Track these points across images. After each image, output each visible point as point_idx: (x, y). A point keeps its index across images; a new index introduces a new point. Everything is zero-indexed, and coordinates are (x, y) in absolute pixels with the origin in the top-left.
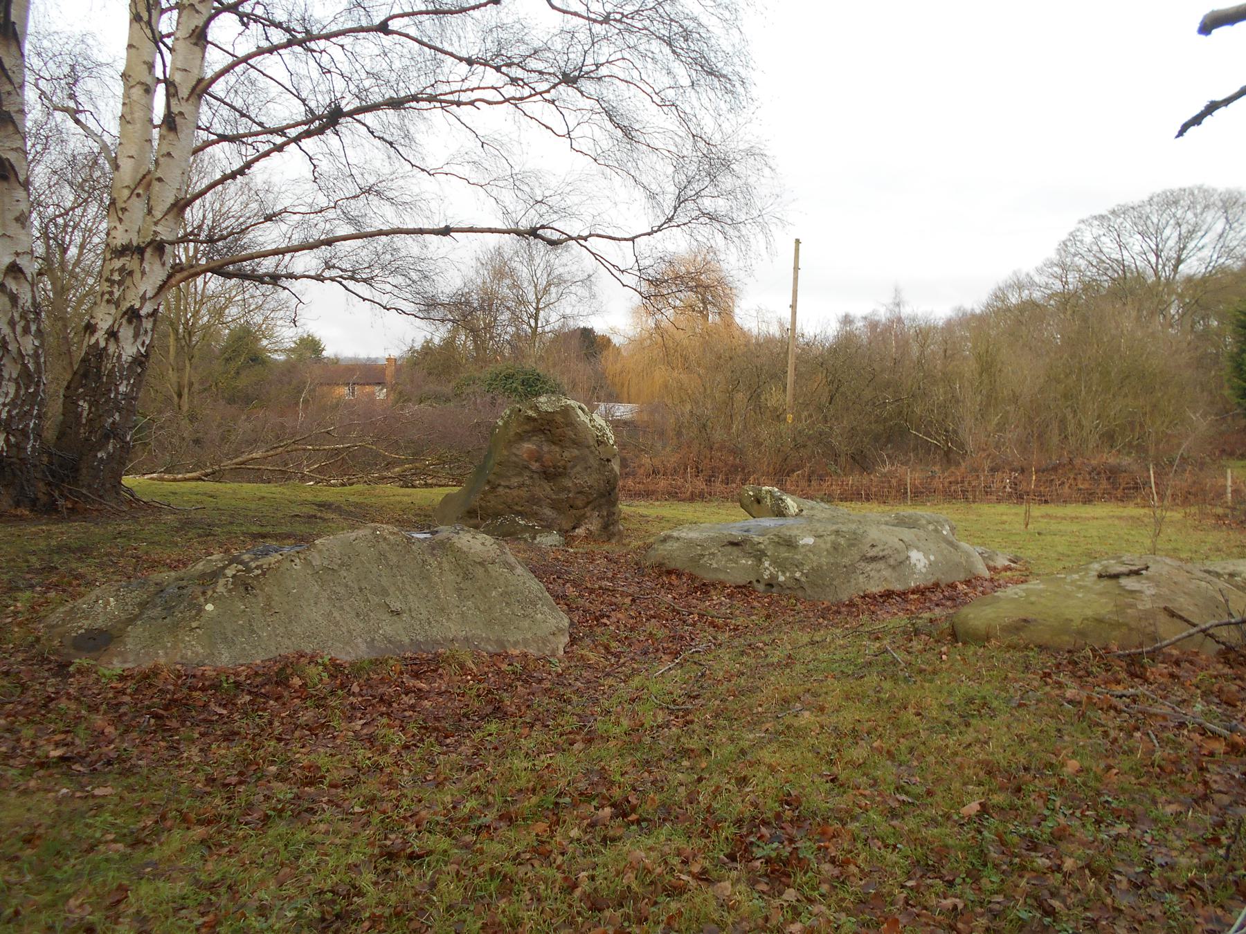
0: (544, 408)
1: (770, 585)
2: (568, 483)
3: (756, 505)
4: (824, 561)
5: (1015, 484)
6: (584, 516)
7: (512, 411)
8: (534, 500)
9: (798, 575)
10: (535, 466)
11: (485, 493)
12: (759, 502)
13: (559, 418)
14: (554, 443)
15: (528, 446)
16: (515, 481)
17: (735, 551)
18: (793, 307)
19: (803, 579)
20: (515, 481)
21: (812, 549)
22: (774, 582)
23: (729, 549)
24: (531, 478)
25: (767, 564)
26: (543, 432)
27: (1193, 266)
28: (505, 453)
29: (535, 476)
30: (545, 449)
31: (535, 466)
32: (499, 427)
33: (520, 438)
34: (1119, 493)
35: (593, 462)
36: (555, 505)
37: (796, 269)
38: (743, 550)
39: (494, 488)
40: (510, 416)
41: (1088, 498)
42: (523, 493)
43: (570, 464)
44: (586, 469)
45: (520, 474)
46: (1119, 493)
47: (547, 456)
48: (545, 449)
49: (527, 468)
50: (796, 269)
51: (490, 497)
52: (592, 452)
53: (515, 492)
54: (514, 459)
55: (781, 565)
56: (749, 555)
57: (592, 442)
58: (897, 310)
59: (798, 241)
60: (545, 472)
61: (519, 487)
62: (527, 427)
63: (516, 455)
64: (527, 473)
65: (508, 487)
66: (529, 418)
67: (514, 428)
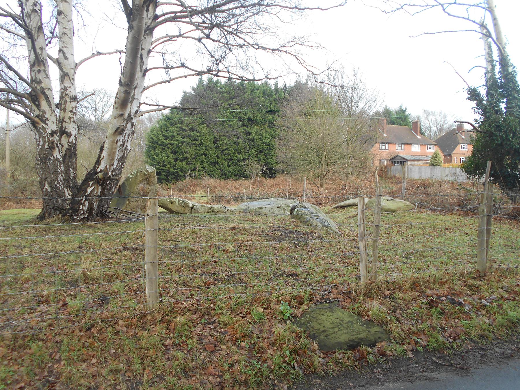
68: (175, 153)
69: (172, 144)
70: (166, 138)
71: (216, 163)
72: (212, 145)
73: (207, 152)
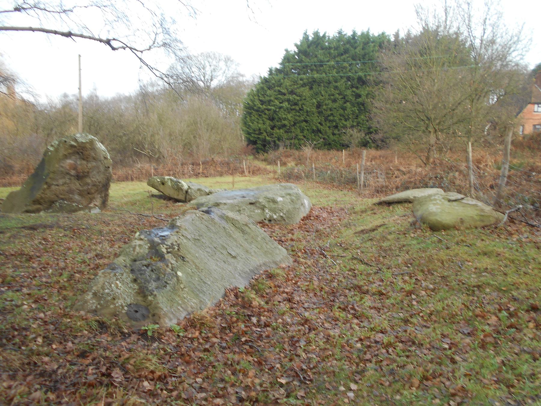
0: (80, 140)
1: (270, 221)
2: (88, 181)
3: (162, 186)
4: (290, 207)
5: (193, 170)
6: (94, 198)
7: (60, 142)
8: (71, 192)
9: (282, 214)
10: (73, 172)
11: (44, 190)
12: (163, 184)
13: (88, 146)
14: (84, 159)
15: (69, 161)
16: (61, 182)
17: (252, 207)
18: (80, 89)
19: (284, 216)
20: (61, 182)
21: (284, 202)
22: (272, 219)
23: (250, 206)
24: (70, 179)
25: (267, 211)
26: (78, 153)
27: (214, 84)
28: (57, 166)
29: (72, 178)
30: (79, 162)
31: (73, 172)
32: (51, 151)
33: (66, 157)
34: (230, 172)
35: (102, 169)
36: (81, 194)
37: (80, 70)
38: (256, 206)
39: (49, 186)
40: (59, 145)
41: (221, 175)
42: (65, 188)
43: (91, 171)
44: (98, 173)
45: (64, 178)
46: (230, 172)
47: (80, 167)
48: (79, 162)
49: (68, 174)
50: (80, 70)
51: (47, 192)
52: (102, 163)
53: (61, 188)
54: (61, 169)
55: (273, 211)
56: (258, 208)
57: (102, 158)
58: (95, 92)
59: (80, 56)
60: (77, 176)
61: (63, 185)
62: (70, 151)
63: (62, 167)
64: (68, 176)
65: (58, 185)
66: (72, 146)
67: (62, 152)
68: (272, 119)
69: (268, 110)
70: (262, 103)
71: (319, 131)
72: (314, 110)
73: (308, 118)
